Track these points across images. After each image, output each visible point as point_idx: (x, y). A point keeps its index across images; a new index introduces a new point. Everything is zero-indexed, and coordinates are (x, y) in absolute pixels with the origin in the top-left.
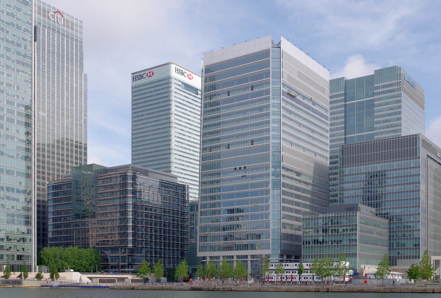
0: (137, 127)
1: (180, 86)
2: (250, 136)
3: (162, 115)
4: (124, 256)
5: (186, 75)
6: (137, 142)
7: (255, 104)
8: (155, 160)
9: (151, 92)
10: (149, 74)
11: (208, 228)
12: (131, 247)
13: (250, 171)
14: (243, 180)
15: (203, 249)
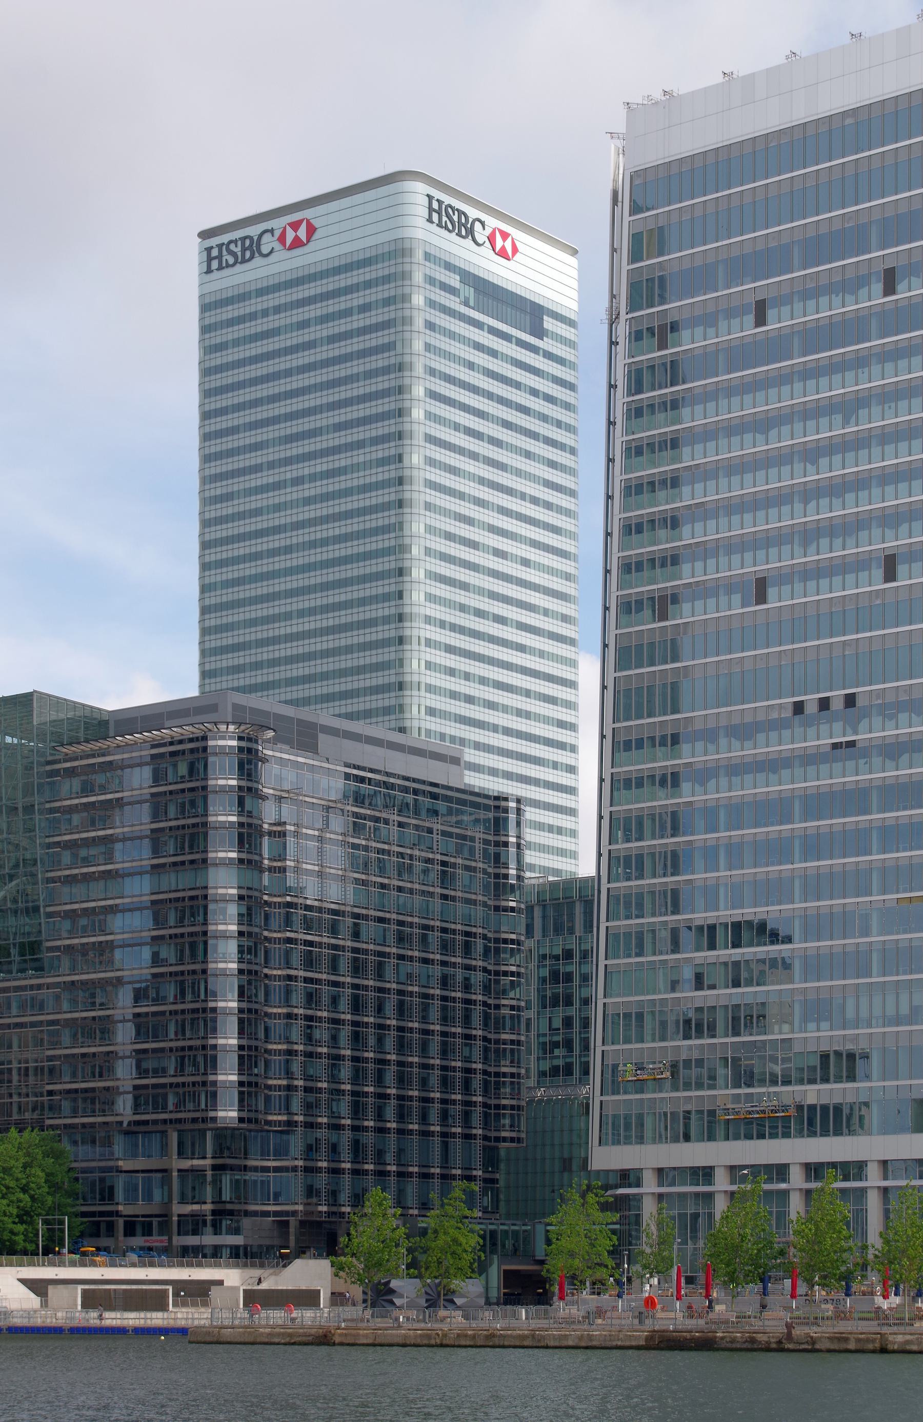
0: (228, 509)
1: (452, 291)
2: (876, 532)
3: (360, 444)
4: (192, 1170)
5: (481, 235)
6: (228, 584)
7: (903, 364)
8: (325, 676)
9: (304, 325)
10: (290, 235)
11: (647, 1019)
12: (235, 1124)
13: (877, 721)
14: (837, 766)
15: (626, 1129)
